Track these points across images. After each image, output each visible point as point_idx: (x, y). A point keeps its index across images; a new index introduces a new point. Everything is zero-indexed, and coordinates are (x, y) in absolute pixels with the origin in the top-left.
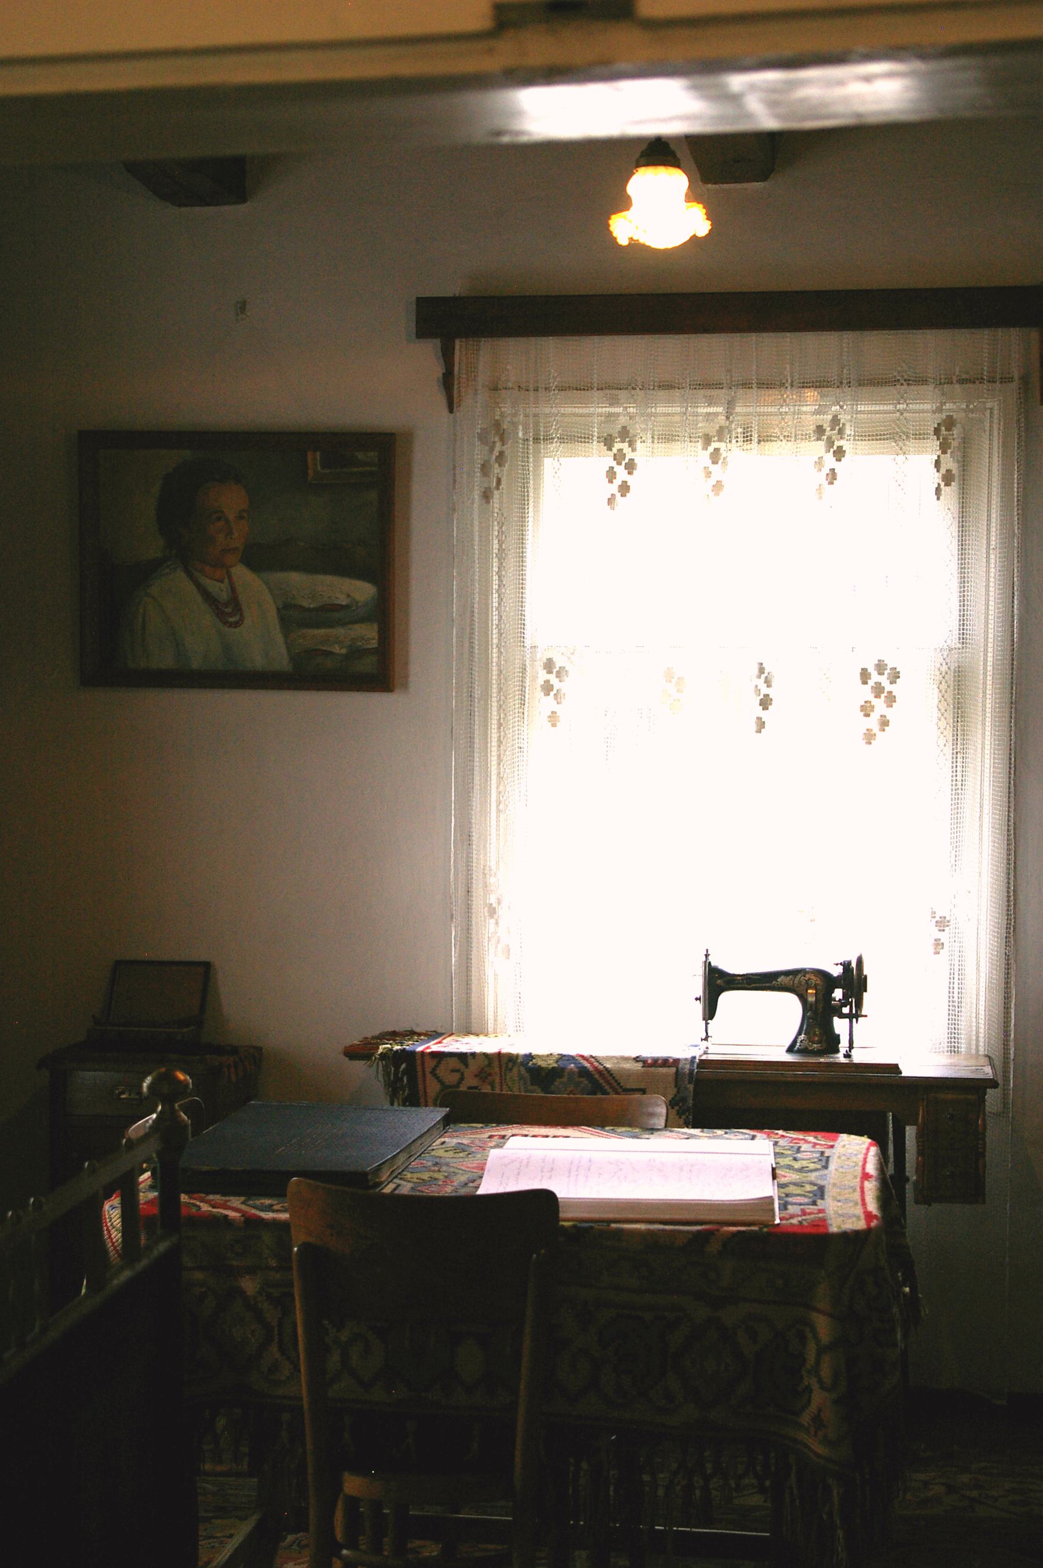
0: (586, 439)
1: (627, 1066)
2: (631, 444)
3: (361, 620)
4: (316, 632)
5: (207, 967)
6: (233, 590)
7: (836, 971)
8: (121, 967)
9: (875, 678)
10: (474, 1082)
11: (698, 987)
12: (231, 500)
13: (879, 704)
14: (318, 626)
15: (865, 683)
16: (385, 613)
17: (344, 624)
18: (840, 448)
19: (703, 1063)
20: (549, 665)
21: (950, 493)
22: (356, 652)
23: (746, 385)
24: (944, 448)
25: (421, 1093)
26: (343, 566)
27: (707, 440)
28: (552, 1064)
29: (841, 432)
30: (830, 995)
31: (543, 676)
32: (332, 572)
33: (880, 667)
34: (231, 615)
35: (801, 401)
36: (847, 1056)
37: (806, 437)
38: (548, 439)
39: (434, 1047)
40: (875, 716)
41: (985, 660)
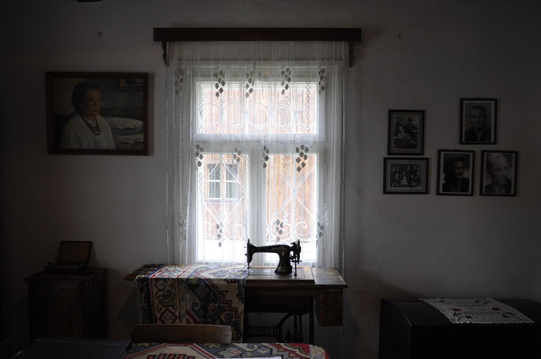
0: (209, 76)
1: (222, 283)
2: (223, 76)
3: (138, 133)
4: (123, 136)
5: (91, 243)
6: (97, 123)
7: (291, 246)
8: (64, 244)
9: (301, 150)
10: (169, 288)
11: (245, 251)
12: (95, 94)
13: (302, 159)
14: (126, 135)
15: (297, 152)
16: (146, 131)
17: (133, 134)
18: (289, 78)
19: (248, 281)
20: (198, 147)
21: (323, 92)
22: (137, 143)
23: (260, 60)
24: (322, 78)
25: (151, 292)
26: (132, 115)
27: (247, 75)
28: (195, 282)
29: (290, 73)
30: (289, 254)
31: (195, 150)
32: (134, 118)
33: (302, 147)
34: (96, 131)
35: (275, 85)
36: (295, 275)
37: (278, 76)
38: (197, 76)
39: (157, 275)
40: (301, 163)
41: (333, 145)
